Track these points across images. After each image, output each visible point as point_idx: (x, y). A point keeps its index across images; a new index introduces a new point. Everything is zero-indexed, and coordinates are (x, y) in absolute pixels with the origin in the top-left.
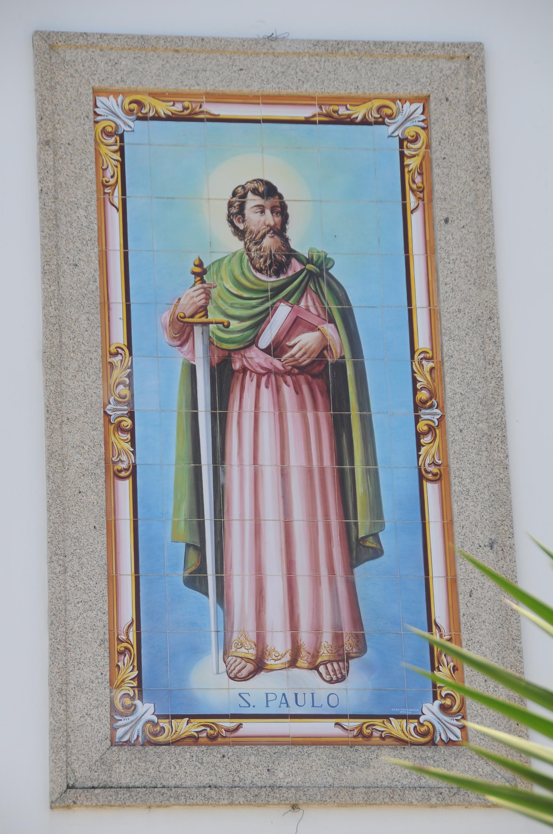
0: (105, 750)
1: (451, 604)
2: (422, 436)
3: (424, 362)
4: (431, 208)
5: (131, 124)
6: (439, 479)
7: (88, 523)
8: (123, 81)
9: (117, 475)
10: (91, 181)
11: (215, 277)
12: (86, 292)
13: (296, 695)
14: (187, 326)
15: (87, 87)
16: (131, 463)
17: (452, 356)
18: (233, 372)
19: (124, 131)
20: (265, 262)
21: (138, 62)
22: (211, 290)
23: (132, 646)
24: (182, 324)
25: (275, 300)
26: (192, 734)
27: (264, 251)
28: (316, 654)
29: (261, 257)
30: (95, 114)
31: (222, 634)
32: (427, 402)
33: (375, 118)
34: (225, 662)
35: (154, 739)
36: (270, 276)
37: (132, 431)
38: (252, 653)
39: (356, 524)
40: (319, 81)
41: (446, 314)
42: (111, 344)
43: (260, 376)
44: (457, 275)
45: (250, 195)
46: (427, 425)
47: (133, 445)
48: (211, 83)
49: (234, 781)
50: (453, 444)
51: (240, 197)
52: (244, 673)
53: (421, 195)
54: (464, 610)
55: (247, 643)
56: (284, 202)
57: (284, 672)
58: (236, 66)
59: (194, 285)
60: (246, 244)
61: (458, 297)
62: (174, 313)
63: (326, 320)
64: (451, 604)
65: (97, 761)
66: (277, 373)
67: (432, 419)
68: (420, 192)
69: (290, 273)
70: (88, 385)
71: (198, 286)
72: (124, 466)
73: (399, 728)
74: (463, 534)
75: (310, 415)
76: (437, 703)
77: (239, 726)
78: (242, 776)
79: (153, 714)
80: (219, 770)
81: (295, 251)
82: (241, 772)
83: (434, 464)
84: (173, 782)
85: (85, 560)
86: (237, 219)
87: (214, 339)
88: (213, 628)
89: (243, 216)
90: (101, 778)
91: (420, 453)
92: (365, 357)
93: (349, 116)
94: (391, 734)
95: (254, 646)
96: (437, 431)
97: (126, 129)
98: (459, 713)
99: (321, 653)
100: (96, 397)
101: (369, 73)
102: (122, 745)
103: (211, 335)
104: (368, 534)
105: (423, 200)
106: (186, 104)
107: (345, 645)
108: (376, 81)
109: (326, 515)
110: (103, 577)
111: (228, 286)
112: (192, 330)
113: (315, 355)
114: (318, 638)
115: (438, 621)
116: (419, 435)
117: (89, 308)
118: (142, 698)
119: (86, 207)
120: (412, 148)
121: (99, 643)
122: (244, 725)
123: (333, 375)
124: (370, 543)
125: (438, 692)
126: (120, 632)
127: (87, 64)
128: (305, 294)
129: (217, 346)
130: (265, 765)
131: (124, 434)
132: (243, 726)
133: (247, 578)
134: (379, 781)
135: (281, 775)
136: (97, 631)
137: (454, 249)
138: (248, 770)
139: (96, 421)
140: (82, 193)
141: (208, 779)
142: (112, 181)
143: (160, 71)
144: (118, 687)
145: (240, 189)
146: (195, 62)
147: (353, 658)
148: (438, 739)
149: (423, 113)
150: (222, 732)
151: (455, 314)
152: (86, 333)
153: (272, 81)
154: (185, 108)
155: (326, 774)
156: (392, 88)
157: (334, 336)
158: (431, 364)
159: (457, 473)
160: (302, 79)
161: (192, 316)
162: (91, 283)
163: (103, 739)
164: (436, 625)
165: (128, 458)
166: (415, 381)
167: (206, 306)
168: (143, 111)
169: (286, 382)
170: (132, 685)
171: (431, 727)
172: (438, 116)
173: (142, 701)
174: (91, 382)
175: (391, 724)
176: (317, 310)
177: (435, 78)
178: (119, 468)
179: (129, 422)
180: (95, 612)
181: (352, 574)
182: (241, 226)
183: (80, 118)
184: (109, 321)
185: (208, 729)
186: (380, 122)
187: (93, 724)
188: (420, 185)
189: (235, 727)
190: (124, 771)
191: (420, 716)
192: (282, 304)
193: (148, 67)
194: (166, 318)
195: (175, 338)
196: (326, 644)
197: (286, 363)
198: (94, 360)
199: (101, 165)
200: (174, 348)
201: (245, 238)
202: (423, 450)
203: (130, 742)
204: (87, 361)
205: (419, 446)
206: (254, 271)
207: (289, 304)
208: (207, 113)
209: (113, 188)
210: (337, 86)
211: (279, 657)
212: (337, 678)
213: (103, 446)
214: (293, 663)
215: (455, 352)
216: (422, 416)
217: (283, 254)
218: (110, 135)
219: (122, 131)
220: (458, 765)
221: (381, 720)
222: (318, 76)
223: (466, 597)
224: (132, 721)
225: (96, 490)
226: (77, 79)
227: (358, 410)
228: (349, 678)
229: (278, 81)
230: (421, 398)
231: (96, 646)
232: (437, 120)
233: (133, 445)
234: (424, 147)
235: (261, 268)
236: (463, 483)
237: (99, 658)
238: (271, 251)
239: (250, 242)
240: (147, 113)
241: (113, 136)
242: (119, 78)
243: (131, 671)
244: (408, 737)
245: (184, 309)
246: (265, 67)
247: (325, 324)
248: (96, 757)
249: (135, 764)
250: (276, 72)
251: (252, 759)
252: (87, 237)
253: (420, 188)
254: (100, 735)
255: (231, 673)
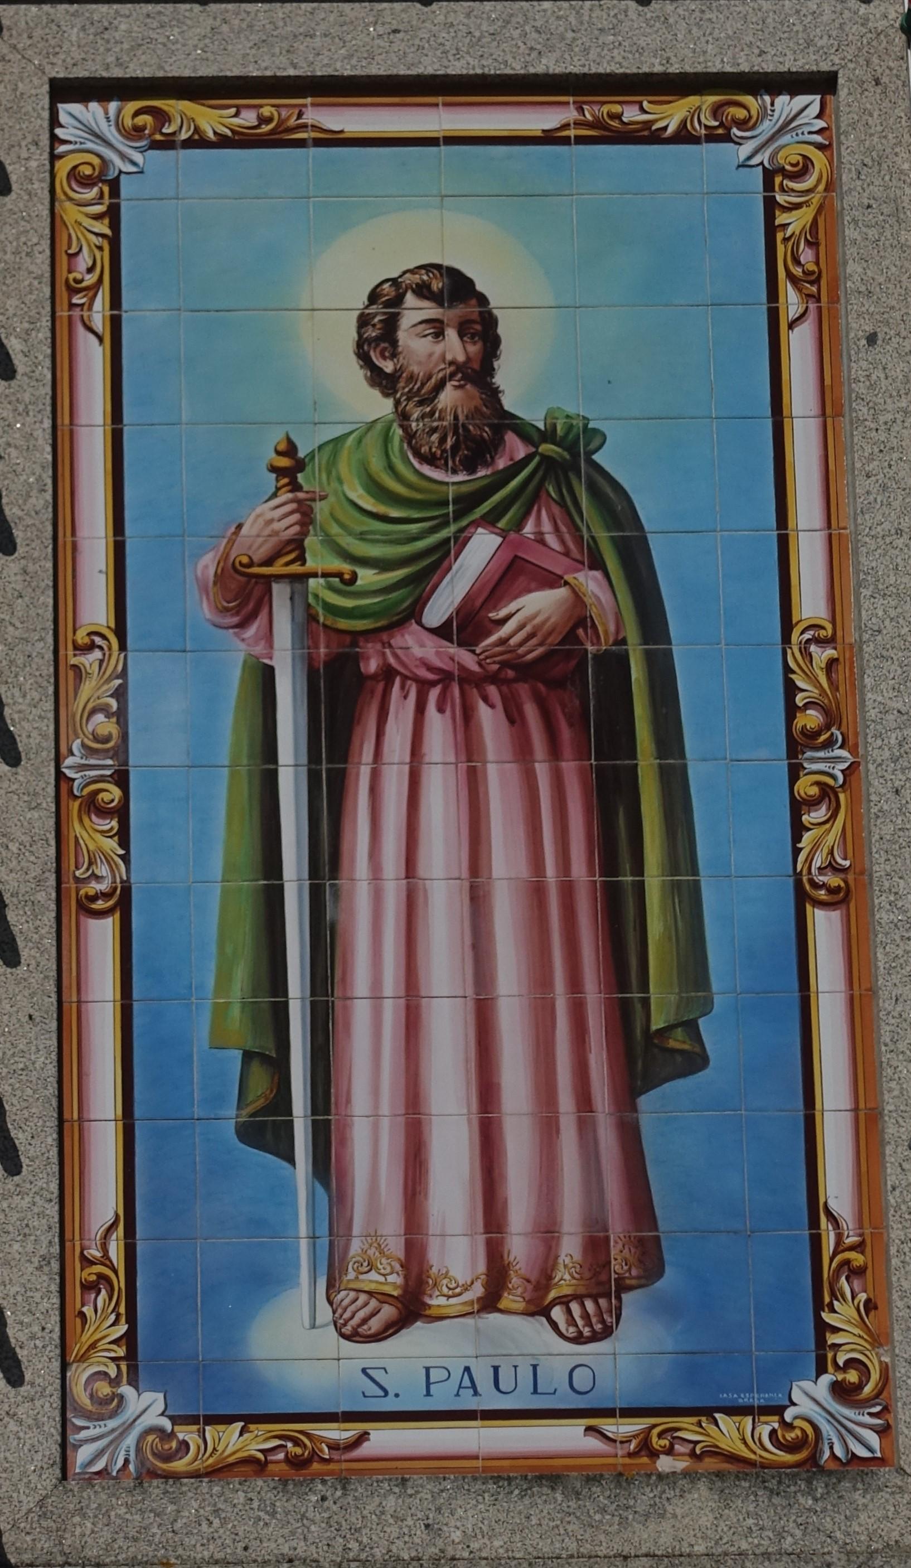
0: (49, 1488)
1: (864, 1169)
2: (804, 808)
3: (813, 648)
4: (834, 316)
5: (138, 157)
6: (845, 901)
7: (15, 1009)
8: (121, 65)
9: (86, 908)
10: (39, 278)
11: (324, 476)
12: (20, 513)
13: (496, 1369)
14: (256, 583)
15: (36, 81)
16: (118, 880)
17: (879, 631)
18: (362, 679)
19: (121, 172)
20: (443, 440)
21: (155, 24)
22: (313, 504)
23: (116, 1272)
24: (243, 579)
25: (464, 523)
26: (251, 1456)
27: (440, 419)
28: (544, 1282)
29: (434, 430)
30: (54, 139)
31: (324, 1242)
32: (818, 733)
33: (706, 127)
34: (331, 1303)
35: (164, 1466)
36: (455, 472)
37: (122, 813)
38: (393, 1282)
39: (646, 1002)
40: (577, 49)
41: (867, 539)
42: (78, 625)
43: (424, 686)
44: (895, 456)
45: (410, 299)
46: (817, 783)
47: (124, 840)
48: (326, 61)
49: (346, 1549)
50: (879, 821)
51: (387, 304)
52: (375, 1325)
53: (814, 289)
54: (894, 1178)
55: (384, 1261)
56: (490, 314)
57: (469, 1321)
58: (383, 24)
59: (275, 495)
60: (397, 403)
61: (896, 504)
62: (226, 555)
63: (583, 563)
64: (864, 1169)
65: (30, 1511)
66: (466, 679)
67: (831, 771)
68: (812, 283)
69: (501, 464)
70: (20, 712)
71: (285, 496)
72: (103, 887)
73: (735, 1435)
74: (896, 1014)
75: (542, 770)
76: (826, 1379)
77: (364, 1437)
78: (365, 1540)
79: (162, 1414)
80: (313, 1528)
81: (513, 416)
82: (364, 1531)
83: (833, 867)
84: (206, 1553)
85: (7, 1087)
86: (378, 350)
87: (320, 611)
88: (303, 1229)
89: (394, 343)
90: (39, 1546)
91: (800, 845)
92: (673, 642)
93: (648, 124)
94: (717, 1447)
95: (398, 1267)
96: (842, 797)
97: (124, 169)
98: (877, 1400)
99: (557, 1279)
100: (39, 739)
101: (695, 30)
102: (90, 1479)
103: (311, 600)
104: (672, 1022)
105: (819, 300)
106: (266, 111)
107: (613, 1262)
108: (710, 46)
109: (575, 983)
110: (48, 1124)
111: (353, 496)
112: (269, 591)
113: (555, 639)
114: (550, 1248)
115: (833, 1205)
116: (797, 806)
117: (27, 548)
118: (137, 1381)
119: (27, 332)
120: (793, 190)
121: (36, 1264)
122: (373, 1435)
123: (596, 680)
124: (678, 1041)
125: (830, 1355)
126: (86, 1243)
127: (38, 33)
128: (536, 508)
129: (325, 626)
130: (419, 1516)
131: (104, 818)
132: (371, 1437)
133: (385, 1123)
134: (685, 1544)
135: (457, 1536)
136: (33, 1238)
137: (889, 401)
138: (380, 1527)
139: (38, 789)
140: (17, 303)
141: (287, 1546)
142: (90, 279)
143: (207, 41)
144: (83, 1358)
145: (386, 286)
146: (288, 19)
147: (630, 1288)
148: (827, 1454)
149: (819, 116)
150: (322, 1451)
151: (888, 540)
152: (20, 600)
153: (468, 53)
154: (263, 120)
155: (562, 1532)
156: (747, 60)
157: (601, 595)
158: (830, 653)
159: (887, 884)
160: (538, 47)
161: (269, 562)
162: (34, 493)
163: (45, 1466)
164: (829, 1214)
165: (112, 870)
166: (791, 689)
167: (303, 540)
168: (164, 131)
169: (486, 699)
170: (113, 1355)
171: (810, 1431)
172: (856, 118)
173: (137, 1388)
174: (29, 705)
175: (717, 1425)
176: (562, 541)
177: (850, 37)
178: (92, 893)
179: (116, 792)
180: (28, 1199)
181: (634, 1109)
182: (388, 367)
183: (20, 146)
184: (74, 577)
185: (290, 1445)
186: (719, 136)
187: (21, 1435)
188: (812, 267)
189: (353, 1439)
190: (93, 1532)
191: (786, 1407)
192: (480, 530)
193: (179, 33)
194: (206, 567)
195: (227, 610)
196: (567, 1260)
197: (487, 658)
198: (36, 660)
199: (65, 248)
200: (225, 631)
201: (396, 392)
202: (807, 837)
203: (108, 1474)
204: (20, 662)
205: (798, 829)
206: (415, 463)
207: (498, 531)
208: (315, 127)
209: (91, 294)
210: (618, 59)
211: (458, 1290)
212: (593, 1331)
213: (53, 842)
214: (490, 1303)
215: (887, 622)
216: (806, 765)
217: (484, 425)
218: (87, 182)
219: (116, 174)
220: (871, 1506)
221: (694, 1420)
222: (574, 39)
223: (899, 1149)
224: (113, 1430)
225: (36, 936)
226: (15, 65)
227: (655, 754)
228: (619, 1332)
229: (480, 53)
230: (804, 727)
231: (30, 1269)
232: (853, 125)
233: (124, 840)
234: (821, 187)
235: (434, 455)
236: (900, 904)
237: (38, 1295)
238: (456, 418)
239: (408, 399)
240: (174, 134)
241: (94, 185)
242: (110, 59)
243: (113, 1325)
244: (755, 1453)
245: (250, 548)
246: (452, 25)
247: (579, 570)
248: (29, 1502)
249: (117, 1516)
250: (477, 34)
251: (391, 1503)
252: (27, 397)
253: (813, 273)
254: (38, 1457)
255: (345, 1325)
